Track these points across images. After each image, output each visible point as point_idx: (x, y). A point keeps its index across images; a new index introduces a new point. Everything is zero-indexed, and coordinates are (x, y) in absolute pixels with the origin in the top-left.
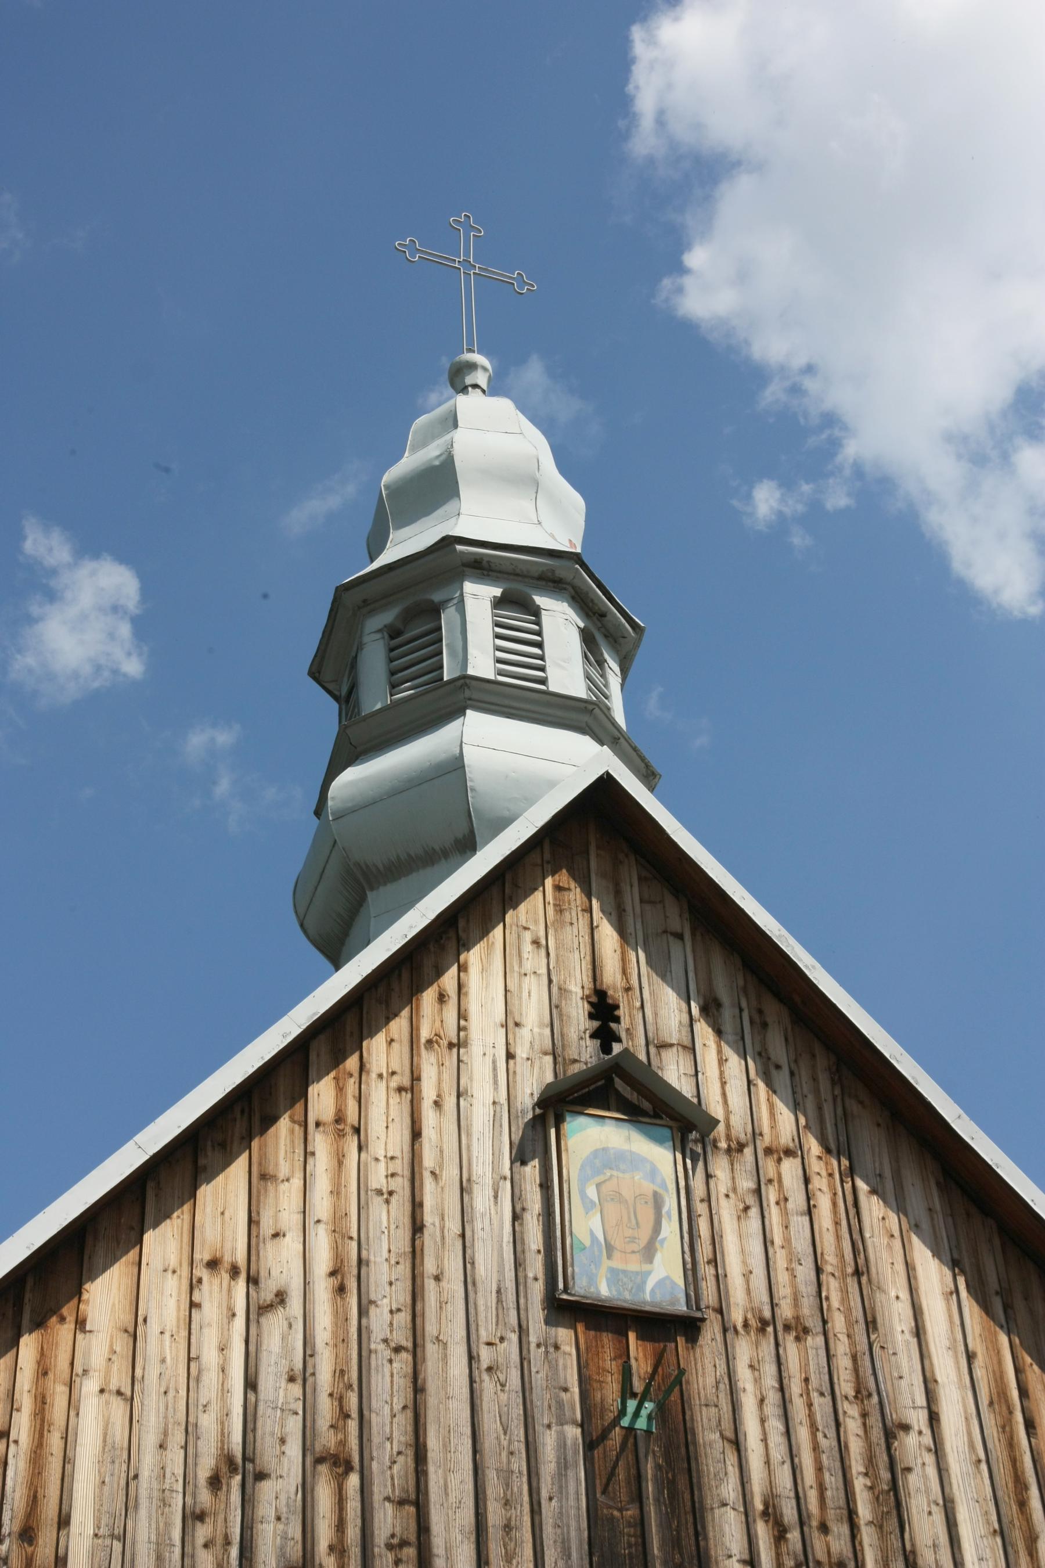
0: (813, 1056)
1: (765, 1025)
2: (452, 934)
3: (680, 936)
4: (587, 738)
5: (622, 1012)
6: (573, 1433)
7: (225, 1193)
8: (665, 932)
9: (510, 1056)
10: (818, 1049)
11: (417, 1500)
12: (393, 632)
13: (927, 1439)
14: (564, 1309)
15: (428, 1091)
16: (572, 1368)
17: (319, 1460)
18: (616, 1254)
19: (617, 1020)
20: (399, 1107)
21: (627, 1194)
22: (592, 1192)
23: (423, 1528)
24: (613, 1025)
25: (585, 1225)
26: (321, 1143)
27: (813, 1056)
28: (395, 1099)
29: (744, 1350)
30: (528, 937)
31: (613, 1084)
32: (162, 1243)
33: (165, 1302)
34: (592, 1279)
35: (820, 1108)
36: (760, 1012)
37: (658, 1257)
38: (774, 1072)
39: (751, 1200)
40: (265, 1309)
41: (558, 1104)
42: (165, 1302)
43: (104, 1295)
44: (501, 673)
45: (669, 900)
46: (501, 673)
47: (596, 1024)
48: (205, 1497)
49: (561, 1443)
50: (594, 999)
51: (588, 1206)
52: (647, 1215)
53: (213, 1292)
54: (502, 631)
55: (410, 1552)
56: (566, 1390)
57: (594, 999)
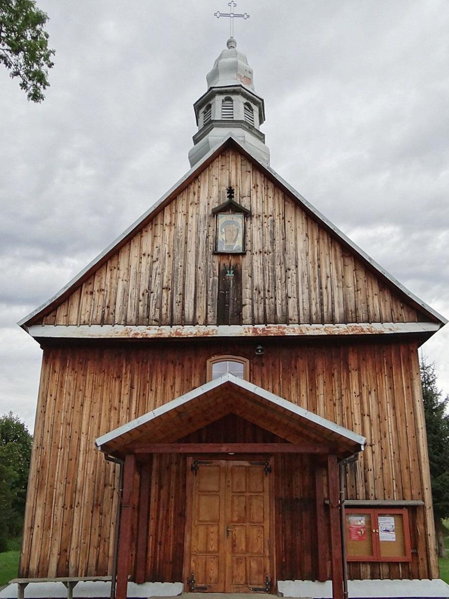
0: (279, 194)
1: (268, 188)
2: (140, 233)
3: (250, 172)
4: (240, 129)
5: (235, 191)
6: (216, 278)
7: (147, 238)
8: (247, 171)
9: (208, 204)
10: (280, 191)
11: (183, 295)
12: (204, 112)
13: (295, 271)
14: (216, 253)
15: (190, 214)
16: (28, 519)
17: (164, 289)
18: (228, 242)
19: (233, 193)
20: (184, 218)
21: (231, 230)
22: (223, 230)
23: (184, 299)
24: (232, 194)
25: (221, 237)
26: (167, 229)
27: (279, 194)
28: (183, 216)
29: (255, 257)
30: (215, 178)
31: (231, 207)
32: (135, 251)
33: (134, 261)
34: (222, 248)
35: (279, 205)
36: (267, 186)
37: (237, 242)
38: (269, 198)
39: (261, 227)
40: (154, 262)
41: (216, 213)
42: (134, 261)
43: (123, 260)
44: (223, 118)
45: (248, 163)
46: (223, 118)
47: (229, 194)
48: (141, 297)
49: (213, 280)
50: (229, 189)
51: (222, 233)
52: (235, 233)
53: (144, 260)
54: (224, 107)
55: (181, 303)
56: (215, 270)
57: (229, 189)
